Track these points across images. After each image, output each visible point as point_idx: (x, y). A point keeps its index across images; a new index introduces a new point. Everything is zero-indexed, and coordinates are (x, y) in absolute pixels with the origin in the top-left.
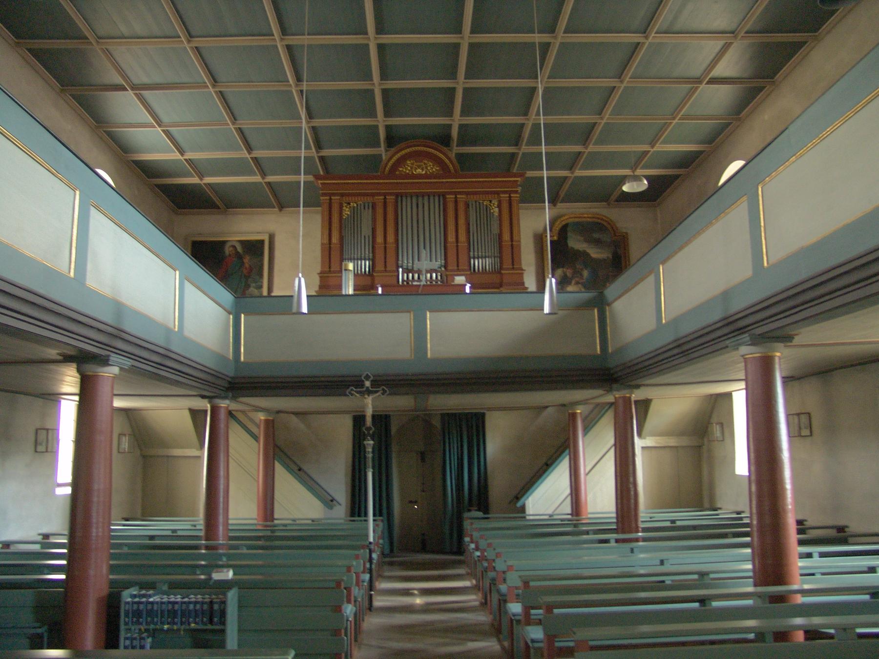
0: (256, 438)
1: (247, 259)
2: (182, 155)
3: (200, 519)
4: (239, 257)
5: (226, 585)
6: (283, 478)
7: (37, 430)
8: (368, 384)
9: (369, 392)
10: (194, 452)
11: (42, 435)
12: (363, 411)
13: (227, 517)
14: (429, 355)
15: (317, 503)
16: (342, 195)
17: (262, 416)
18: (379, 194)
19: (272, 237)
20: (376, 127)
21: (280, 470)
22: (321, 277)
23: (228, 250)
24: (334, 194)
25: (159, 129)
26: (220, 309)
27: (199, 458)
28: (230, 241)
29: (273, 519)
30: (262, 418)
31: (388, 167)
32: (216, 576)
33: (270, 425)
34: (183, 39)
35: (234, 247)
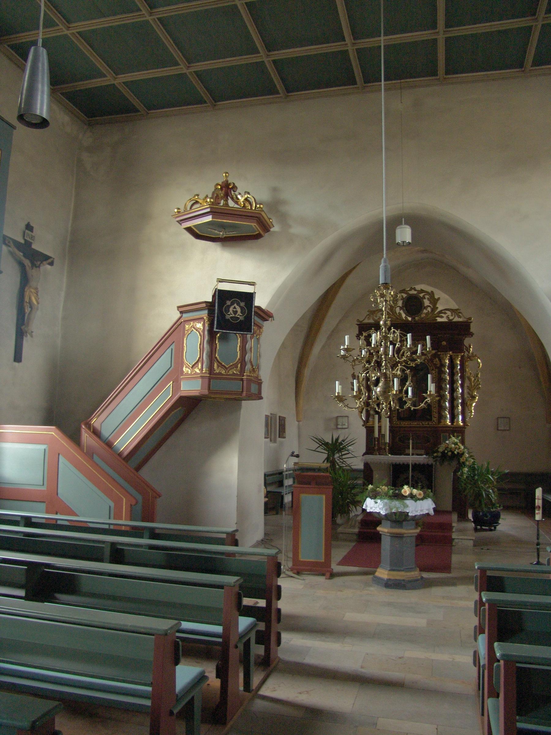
20: (345, 53)
34: (144, 12)
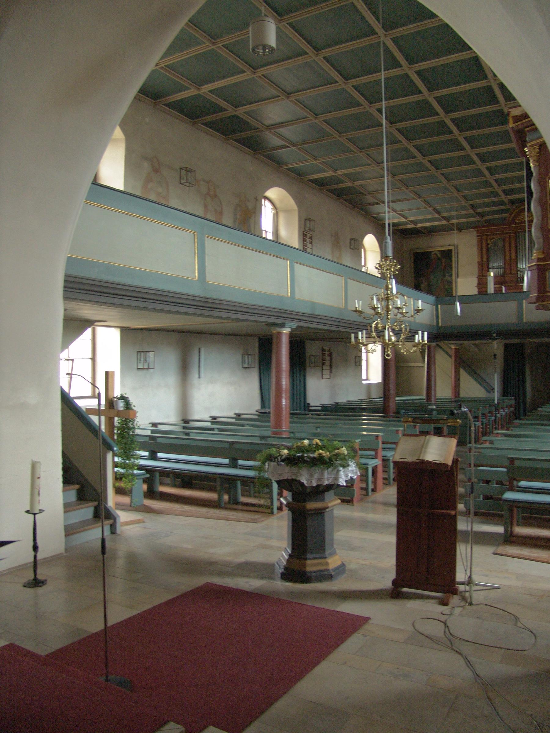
0: (450, 356)
1: (443, 260)
2: (406, 219)
3: (424, 396)
4: (438, 258)
5: (433, 410)
6: (464, 376)
7: (356, 357)
8: (495, 335)
9: (495, 339)
10: (420, 364)
11: (357, 359)
12: (291, 422)
13: (435, 394)
14: (525, 320)
15: (483, 390)
16: (487, 235)
17: (453, 347)
18: (507, 233)
19: (457, 247)
21: (462, 372)
22: (478, 279)
23: (433, 256)
24: (483, 235)
25: (395, 213)
26: (429, 305)
27: (423, 367)
28: (433, 251)
29: (459, 397)
30: (453, 347)
31: (511, 218)
32: (430, 407)
33: (457, 351)
35: (436, 254)
